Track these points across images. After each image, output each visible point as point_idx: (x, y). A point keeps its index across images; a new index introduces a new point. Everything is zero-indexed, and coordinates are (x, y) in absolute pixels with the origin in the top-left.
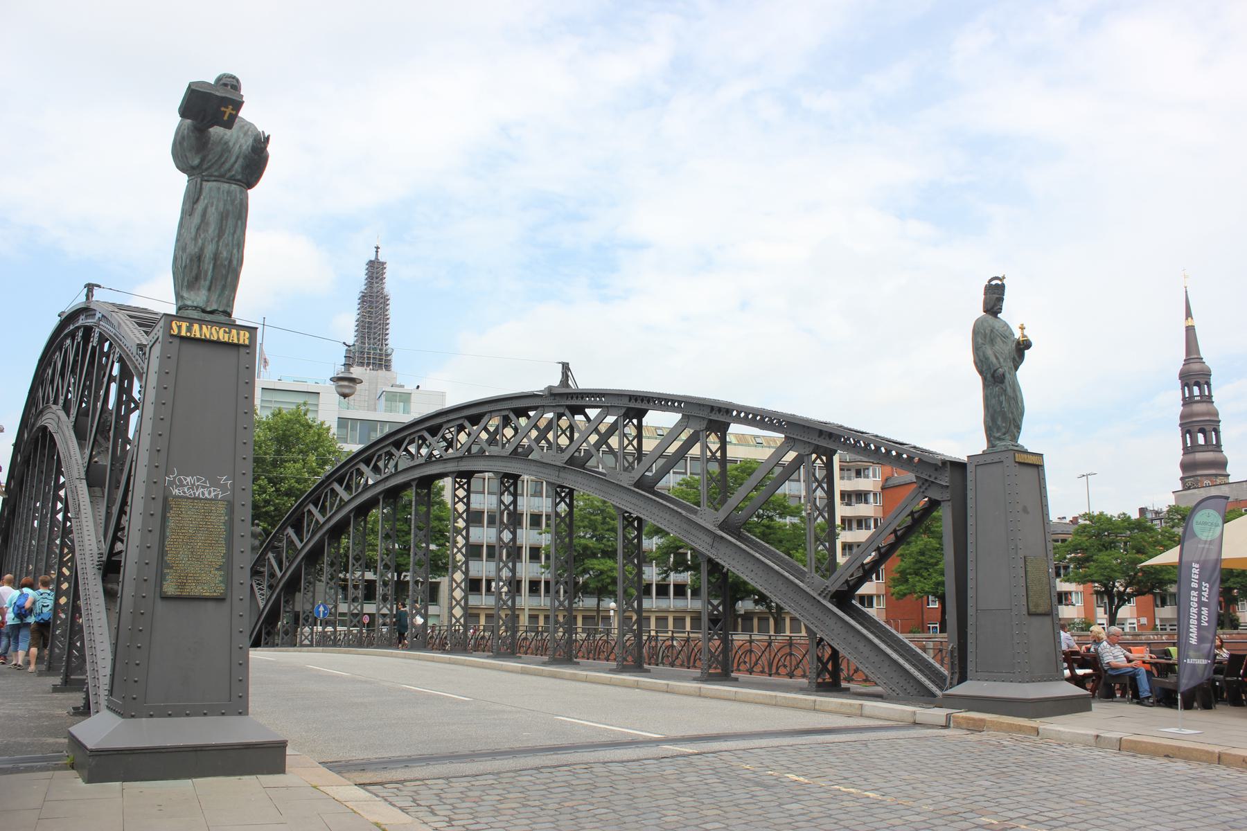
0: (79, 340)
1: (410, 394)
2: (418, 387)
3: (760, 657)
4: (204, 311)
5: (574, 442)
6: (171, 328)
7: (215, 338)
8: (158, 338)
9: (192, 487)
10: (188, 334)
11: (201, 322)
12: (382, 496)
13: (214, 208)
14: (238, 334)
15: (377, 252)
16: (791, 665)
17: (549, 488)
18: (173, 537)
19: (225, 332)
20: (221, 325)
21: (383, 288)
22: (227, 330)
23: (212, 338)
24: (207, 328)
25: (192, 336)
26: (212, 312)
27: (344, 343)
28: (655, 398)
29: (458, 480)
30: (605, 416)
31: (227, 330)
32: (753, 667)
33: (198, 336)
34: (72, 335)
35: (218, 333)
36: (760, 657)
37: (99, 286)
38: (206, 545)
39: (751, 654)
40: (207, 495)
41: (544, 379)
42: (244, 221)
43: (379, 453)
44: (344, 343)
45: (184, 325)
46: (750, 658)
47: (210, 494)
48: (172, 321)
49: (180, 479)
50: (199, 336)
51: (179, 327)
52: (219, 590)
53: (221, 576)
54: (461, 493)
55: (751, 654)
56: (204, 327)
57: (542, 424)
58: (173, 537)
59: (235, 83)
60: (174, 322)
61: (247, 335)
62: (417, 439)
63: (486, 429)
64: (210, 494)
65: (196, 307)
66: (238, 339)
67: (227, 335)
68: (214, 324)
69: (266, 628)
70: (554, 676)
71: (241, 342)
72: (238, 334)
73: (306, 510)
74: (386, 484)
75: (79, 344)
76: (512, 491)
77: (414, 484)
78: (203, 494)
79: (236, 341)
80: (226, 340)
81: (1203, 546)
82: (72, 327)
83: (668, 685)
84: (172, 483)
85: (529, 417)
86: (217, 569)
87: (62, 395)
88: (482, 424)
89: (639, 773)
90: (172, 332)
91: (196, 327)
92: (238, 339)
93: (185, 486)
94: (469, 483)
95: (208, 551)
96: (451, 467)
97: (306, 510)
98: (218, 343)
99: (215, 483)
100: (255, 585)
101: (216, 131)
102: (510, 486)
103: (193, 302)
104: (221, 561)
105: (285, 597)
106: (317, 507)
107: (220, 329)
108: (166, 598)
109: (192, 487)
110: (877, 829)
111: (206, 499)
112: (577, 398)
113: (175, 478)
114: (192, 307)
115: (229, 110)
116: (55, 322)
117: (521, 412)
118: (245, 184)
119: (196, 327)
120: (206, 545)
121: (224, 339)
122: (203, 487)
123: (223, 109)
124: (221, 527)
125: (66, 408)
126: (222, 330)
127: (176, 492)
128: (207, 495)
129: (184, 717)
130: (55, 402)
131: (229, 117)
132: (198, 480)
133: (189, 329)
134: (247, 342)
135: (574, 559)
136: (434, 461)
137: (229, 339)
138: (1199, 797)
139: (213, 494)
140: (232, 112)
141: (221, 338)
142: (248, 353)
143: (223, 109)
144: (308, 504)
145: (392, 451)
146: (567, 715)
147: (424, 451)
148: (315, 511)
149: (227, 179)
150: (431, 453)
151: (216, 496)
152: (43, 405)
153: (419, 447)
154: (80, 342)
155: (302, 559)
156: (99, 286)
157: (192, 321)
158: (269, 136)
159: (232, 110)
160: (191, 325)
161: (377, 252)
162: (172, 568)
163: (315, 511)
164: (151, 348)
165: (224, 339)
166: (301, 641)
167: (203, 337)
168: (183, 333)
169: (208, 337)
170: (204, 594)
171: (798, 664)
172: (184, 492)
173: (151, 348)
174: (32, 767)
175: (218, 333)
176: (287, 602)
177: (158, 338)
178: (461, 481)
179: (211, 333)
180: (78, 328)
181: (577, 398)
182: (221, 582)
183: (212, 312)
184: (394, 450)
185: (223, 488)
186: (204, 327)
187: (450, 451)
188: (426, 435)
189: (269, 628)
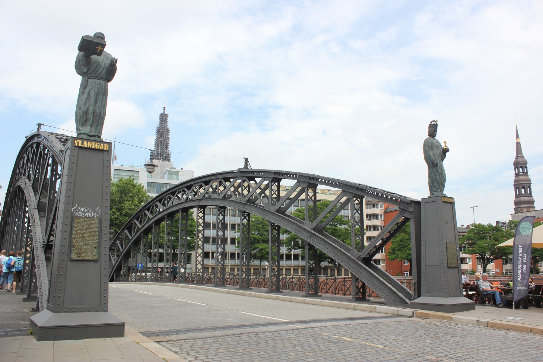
0: (34, 148)
1: (179, 171)
2: (182, 169)
3: (331, 286)
4: (89, 136)
5: (250, 193)
6: (75, 143)
7: (94, 147)
8: (69, 147)
9: (84, 212)
10: (82, 146)
11: (88, 140)
12: (166, 216)
13: (93, 90)
14: (104, 146)
15: (164, 110)
16: (344, 289)
17: (239, 213)
18: (75, 234)
19: (98, 145)
20: (96, 142)
21: (167, 126)
22: (99, 144)
23: (92, 147)
24: (90, 143)
25: (84, 146)
26: (92, 136)
28: (285, 173)
29: (200, 209)
30: (263, 181)
31: (99, 144)
33: (86, 146)
34: (32, 146)
35: (95, 145)
36: (331, 286)
37: (43, 125)
38: (90, 237)
39: (327, 285)
40: (90, 216)
41: (237, 165)
42: (106, 96)
43: (165, 197)
45: (80, 142)
46: (327, 287)
47: (91, 215)
48: (75, 140)
49: (78, 209)
50: (87, 147)
51: (78, 143)
52: (96, 257)
53: (96, 251)
54: (201, 215)
55: (327, 285)
56: (89, 142)
57: (236, 185)
58: (75, 234)
59: (102, 36)
60: (76, 140)
61: (108, 146)
62: (181, 191)
63: (211, 187)
64: (91, 215)
65: (85, 134)
66: (104, 148)
67: (99, 146)
68: (93, 141)
69: (116, 274)
70: (241, 294)
71: (105, 149)
72: (104, 146)
73: (133, 222)
74: (168, 211)
75: (34, 150)
76: (223, 214)
77: (180, 211)
78: (88, 215)
79: (103, 149)
80: (99, 148)
81: (524, 238)
82: (31, 143)
84: (75, 210)
85: (230, 182)
86: (94, 248)
87: (27, 172)
88: (210, 185)
89: (278, 337)
90: (75, 145)
91: (85, 142)
92: (104, 148)
93: (80, 212)
94: (204, 210)
95: (90, 240)
96: (196, 203)
97: (133, 222)
98: (95, 149)
99: (94, 211)
100: (111, 255)
101: (94, 57)
102: (222, 212)
103: (84, 132)
104: (96, 244)
105: (124, 260)
106: (138, 221)
107: (96, 143)
108: (72, 261)
109: (84, 212)
111: (90, 217)
112: (251, 173)
113: (76, 208)
114: (84, 134)
115: (100, 48)
116: (24, 140)
117: (227, 180)
118: (107, 80)
119: (85, 142)
120: (90, 237)
121: (97, 147)
122: (89, 212)
123: (97, 47)
124: (96, 230)
125: (29, 178)
126: (97, 144)
127: (77, 214)
128: (90, 216)
129: (80, 312)
130: (24, 175)
131: (100, 51)
132: (86, 209)
133: (82, 143)
134: (107, 149)
135: (250, 244)
136: (189, 201)
137: (100, 147)
138: (522, 347)
139: (93, 215)
140: (101, 49)
141: (96, 147)
142: (108, 154)
143: (97, 47)
144: (134, 220)
145: (171, 196)
146: (247, 312)
147: (185, 197)
148: (137, 223)
149: (99, 78)
150: (188, 197)
151: (94, 216)
152: (19, 176)
153: (183, 195)
154: (35, 149)
155: (132, 243)
156: (43, 125)
157: (84, 140)
158: (117, 59)
159: (101, 48)
160: (83, 142)
161: (164, 110)
162: (75, 247)
163: (137, 223)
164: (66, 152)
165: (97, 147)
166: (131, 279)
167: (88, 147)
168: (80, 145)
169: (91, 147)
170: (89, 259)
171: (347, 289)
172: (80, 214)
173: (66, 152)
174: (14, 334)
175: (95, 145)
176: (125, 262)
177: (69, 147)
178: (201, 210)
179: (92, 145)
180: (34, 143)
181: (251, 173)
182: (96, 253)
183: (92, 136)
184: (171, 196)
185: (97, 213)
186: (89, 142)
187: (196, 196)
188: (186, 189)
189: (117, 274)
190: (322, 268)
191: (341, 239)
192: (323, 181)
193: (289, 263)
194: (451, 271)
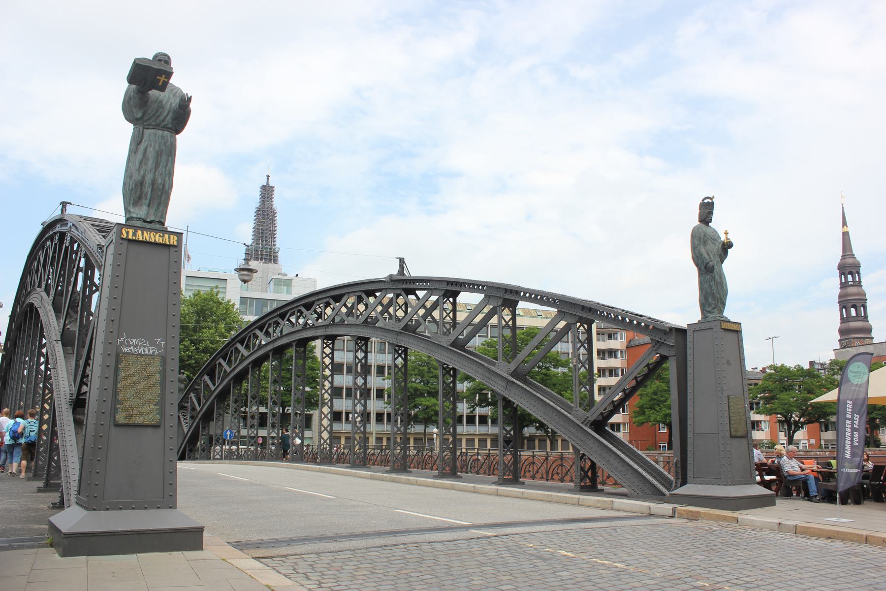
0: (56, 242)
1: (292, 280)
2: (297, 275)
3: (540, 467)
4: (145, 221)
6: (122, 233)
7: (153, 241)
8: (112, 241)
9: (137, 346)
10: (134, 238)
11: (143, 229)
12: (272, 352)
13: (152, 148)
14: (169, 238)
15: (268, 179)
16: (562, 473)
17: (390, 347)
18: (123, 382)
19: (160, 236)
20: (157, 231)
21: (272, 205)
22: (161, 234)
23: (151, 241)
24: (147, 233)
25: (137, 239)
26: (150, 222)
27: (245, 244)
28: (466, 283)
29: (326, 341)
30: (430, 296)
31: (161, 234)
32: (535, 474)
33: (141, 239)
34: (51, 238)
35: (155, 236)
36: (540, 467)
37: (70, 204)
38: (146, 387)
39: (533, 465)
40: (147, 352)
41: (387, 270)
43: (269, 322)
44: (245, 244)
45: (131, 231)
46: (533, 468)
47: (149, 351)
48: (122, 229)
49: (128, 341)
50: (141, 239)
51: (128, 233)
52: (156, 420)
53: (157, 410)
54: (328, 351)
55: (533, 465)
56: (145, 232)
57: (385, 301)
58: (123, 382)
59: (167, 59)
60: (124, 229)
61: (176, 238)
62: (296, 312)
63: (345, 305)
64: (149, 351)
65: (139, 219)
66: (169, 241)
67: (161, 239)
68: (152, 230)
69: (189, 447)
71: (171, 243)
72: (169, 238)
73: (217, 363)
74: (275, 344)
75: (56, 244)
76: (364, 349)
77: (294, 344)
78: (144, 351)
79: (167, 243)
80: (161, 241)
82: (51, 233)
83: (474, 487)
84: (122, 344)
85: (376, 297)
86: (154, 405)
87: (44, 281)
88: (343, 301)
89: (454, 550)
90: (122, 236)
91: (139, 232)
92: (169, 241)
93: (131, 345)
94: (333, 344)
95: (148, 392)
96: (320, 332)
97: (217, 363)
98: (155, 244)
99: (153, 344)
100: (181, 416)
101: (153, 93)
102: (362, 346)
103: (137, 215)
104: (157, 399)
105: (202, 425)
106: (225, 361)
107: (156, 234)
108: (118, 425)
109: (137, 346)
110: (623, 589)
111: (146, 355)
112: (410, 283)
113: (124, 340)
114: (136, 218)
115: (163, 79)
116: (39, 229)
117: (370, 293)
118: (174, 131)
119: (139, 232)
120: (146, 387)
121: (159, 241)
122: (144, 346)
123: (158, 77)
124: (157, 375)
125: (47, 290)
126: (158, 235)
127: (125, 350)
128: (147, 352)
129: (131, 510)
130: (39, 286)
131: (162, 83)
132: (141, 341)
133: (134, 234)
134: (175, 243)
135: (408, 398)
136: (308, 328)
137: (163, 241)
139: (151, 351)
140: (165, 80)
141: (157, 240)
142: (176, 251)
143: (158, 77)
144: (219, 359)
145: (278, 320)
147: (301, 321)
148: (224, 364)
149: (162, 127)
150: (307, 322)
151: (154, 352)
152: (30, 288)
153: (298, 318)
154: (57, 243)
155: (215, 397)
156: (70, 204)
157: (136, 228)
158: (191, 97)
159: (165, 78)
160: (136, 231)
161: (268, 179)
162: (122, 404)
163: (224, 364)
164: (107, 248)
165: (159, 241)
166: (214, 456)
167: (144, 240)
168: (130, 237)
169: (148, 239)
170: (145, 423)
171: (567, 472)
172: (131, 350)
173: (107, 248)
174: (23, 545)
175: (155, 236)
176: (204, 428)
177: (112, 241)
178: (327, 342)
179: (150, 237)
180: (56, 233)
181: (410, 283)
182: (157, 414)
183: (150, 222)
184: (280, 320)
185: (159, 347)
186: (145, 232)
187: (320, 320)
188: (303, 309)
189: (191, 447)
190: (526, 438)
191: (556, 390)
192: (528, 295)
193: (471, 429)
194: (736, 442)
